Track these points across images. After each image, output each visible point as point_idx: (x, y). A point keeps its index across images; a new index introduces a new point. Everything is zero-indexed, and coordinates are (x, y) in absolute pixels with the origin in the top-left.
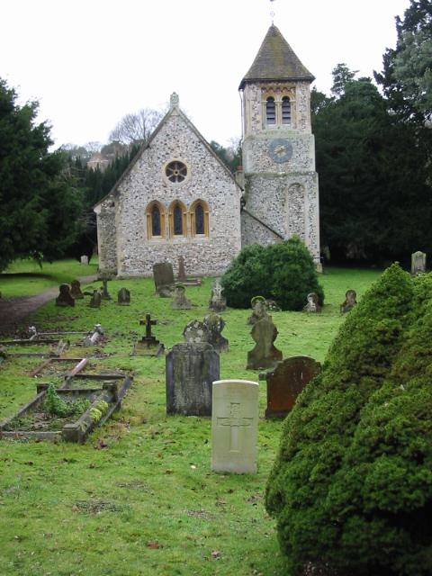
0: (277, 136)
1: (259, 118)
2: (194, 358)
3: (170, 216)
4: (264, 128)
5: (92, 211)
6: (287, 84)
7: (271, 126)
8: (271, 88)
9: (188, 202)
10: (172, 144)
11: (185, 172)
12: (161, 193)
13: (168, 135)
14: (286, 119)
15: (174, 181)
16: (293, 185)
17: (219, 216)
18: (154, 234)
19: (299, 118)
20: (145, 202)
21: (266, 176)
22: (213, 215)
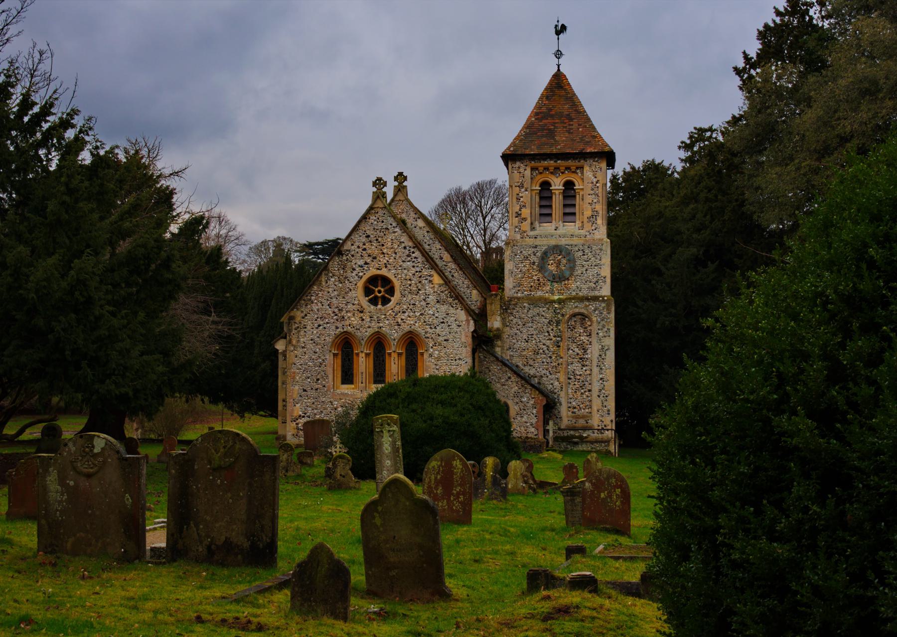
0: (553, 242)
1: (526, 212)
2: (536, 380)
3: (367, 355)
4: (533, 229)
5: (273, 345)
6: (570, 163)
7: (548, 228)
8: (546, 169)
9: (394, 334)
10: (373, 249)
11: (391, 291)
12: (355, 321)
13: (368, 236)
14: (569, 215)
15: (376, 304)
16: (574, 315)
17: (438, 359)
18: (343, 383)
19: (588, 213)
20: (331, 332)
21: (535, 302)
22: (431, 355)
